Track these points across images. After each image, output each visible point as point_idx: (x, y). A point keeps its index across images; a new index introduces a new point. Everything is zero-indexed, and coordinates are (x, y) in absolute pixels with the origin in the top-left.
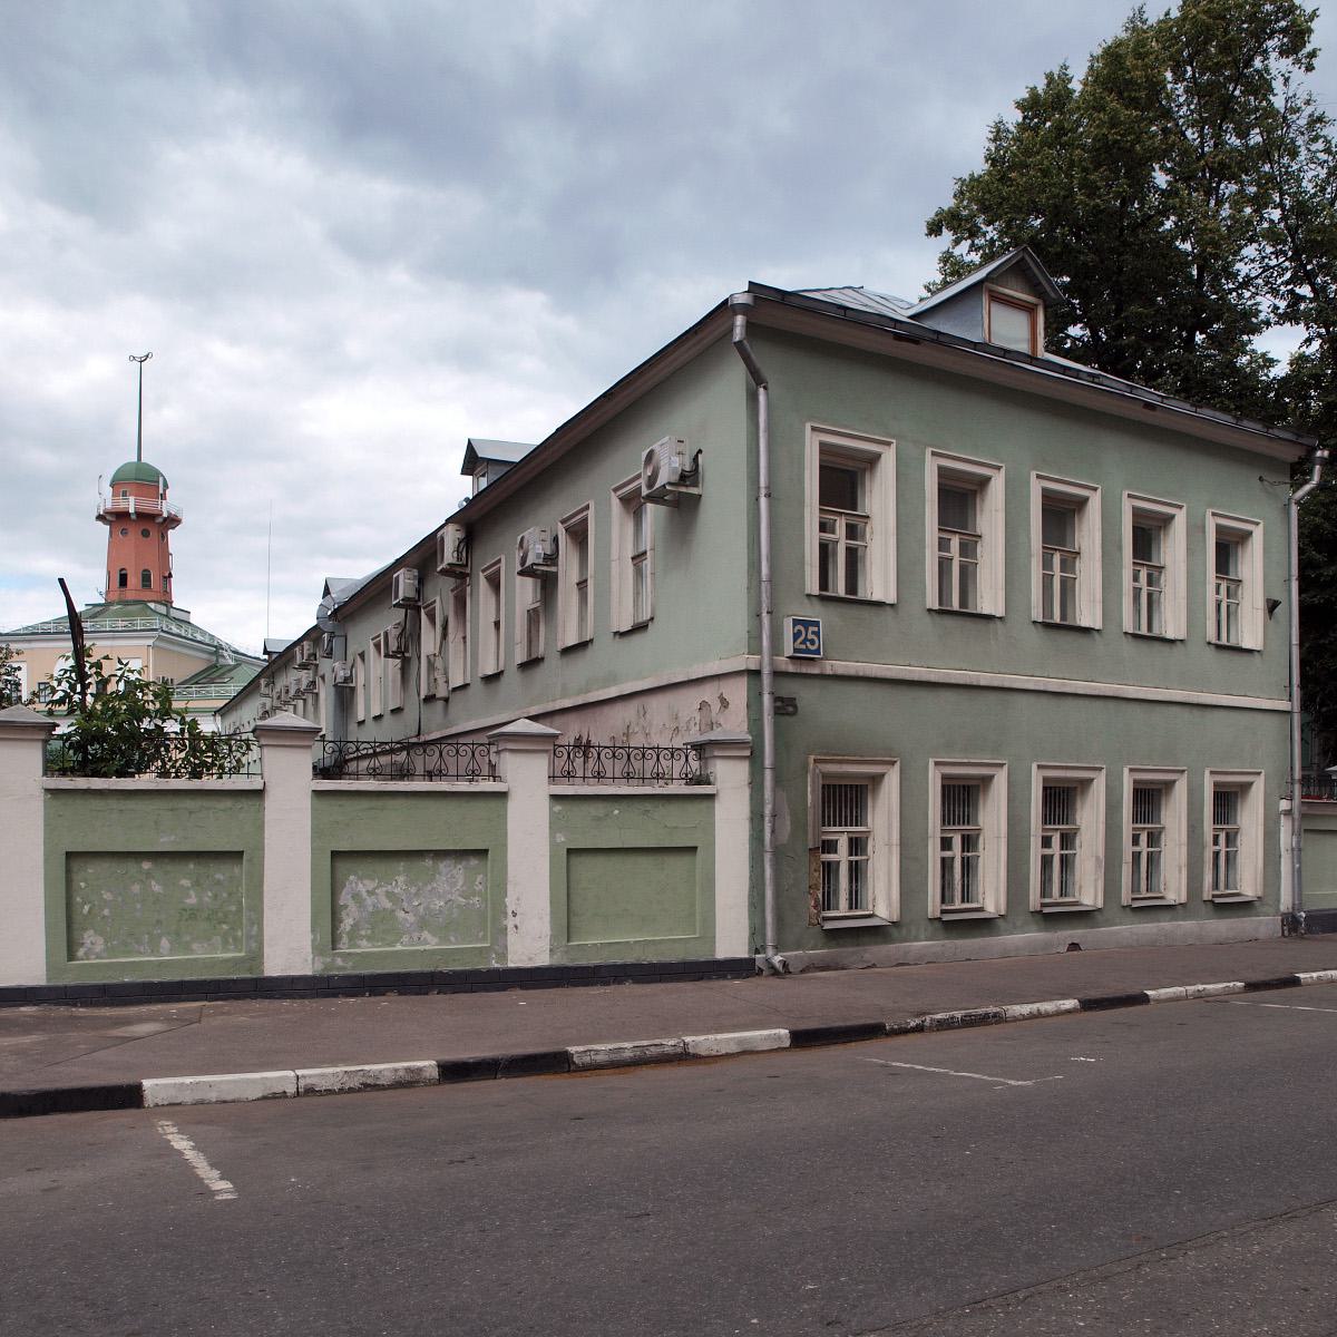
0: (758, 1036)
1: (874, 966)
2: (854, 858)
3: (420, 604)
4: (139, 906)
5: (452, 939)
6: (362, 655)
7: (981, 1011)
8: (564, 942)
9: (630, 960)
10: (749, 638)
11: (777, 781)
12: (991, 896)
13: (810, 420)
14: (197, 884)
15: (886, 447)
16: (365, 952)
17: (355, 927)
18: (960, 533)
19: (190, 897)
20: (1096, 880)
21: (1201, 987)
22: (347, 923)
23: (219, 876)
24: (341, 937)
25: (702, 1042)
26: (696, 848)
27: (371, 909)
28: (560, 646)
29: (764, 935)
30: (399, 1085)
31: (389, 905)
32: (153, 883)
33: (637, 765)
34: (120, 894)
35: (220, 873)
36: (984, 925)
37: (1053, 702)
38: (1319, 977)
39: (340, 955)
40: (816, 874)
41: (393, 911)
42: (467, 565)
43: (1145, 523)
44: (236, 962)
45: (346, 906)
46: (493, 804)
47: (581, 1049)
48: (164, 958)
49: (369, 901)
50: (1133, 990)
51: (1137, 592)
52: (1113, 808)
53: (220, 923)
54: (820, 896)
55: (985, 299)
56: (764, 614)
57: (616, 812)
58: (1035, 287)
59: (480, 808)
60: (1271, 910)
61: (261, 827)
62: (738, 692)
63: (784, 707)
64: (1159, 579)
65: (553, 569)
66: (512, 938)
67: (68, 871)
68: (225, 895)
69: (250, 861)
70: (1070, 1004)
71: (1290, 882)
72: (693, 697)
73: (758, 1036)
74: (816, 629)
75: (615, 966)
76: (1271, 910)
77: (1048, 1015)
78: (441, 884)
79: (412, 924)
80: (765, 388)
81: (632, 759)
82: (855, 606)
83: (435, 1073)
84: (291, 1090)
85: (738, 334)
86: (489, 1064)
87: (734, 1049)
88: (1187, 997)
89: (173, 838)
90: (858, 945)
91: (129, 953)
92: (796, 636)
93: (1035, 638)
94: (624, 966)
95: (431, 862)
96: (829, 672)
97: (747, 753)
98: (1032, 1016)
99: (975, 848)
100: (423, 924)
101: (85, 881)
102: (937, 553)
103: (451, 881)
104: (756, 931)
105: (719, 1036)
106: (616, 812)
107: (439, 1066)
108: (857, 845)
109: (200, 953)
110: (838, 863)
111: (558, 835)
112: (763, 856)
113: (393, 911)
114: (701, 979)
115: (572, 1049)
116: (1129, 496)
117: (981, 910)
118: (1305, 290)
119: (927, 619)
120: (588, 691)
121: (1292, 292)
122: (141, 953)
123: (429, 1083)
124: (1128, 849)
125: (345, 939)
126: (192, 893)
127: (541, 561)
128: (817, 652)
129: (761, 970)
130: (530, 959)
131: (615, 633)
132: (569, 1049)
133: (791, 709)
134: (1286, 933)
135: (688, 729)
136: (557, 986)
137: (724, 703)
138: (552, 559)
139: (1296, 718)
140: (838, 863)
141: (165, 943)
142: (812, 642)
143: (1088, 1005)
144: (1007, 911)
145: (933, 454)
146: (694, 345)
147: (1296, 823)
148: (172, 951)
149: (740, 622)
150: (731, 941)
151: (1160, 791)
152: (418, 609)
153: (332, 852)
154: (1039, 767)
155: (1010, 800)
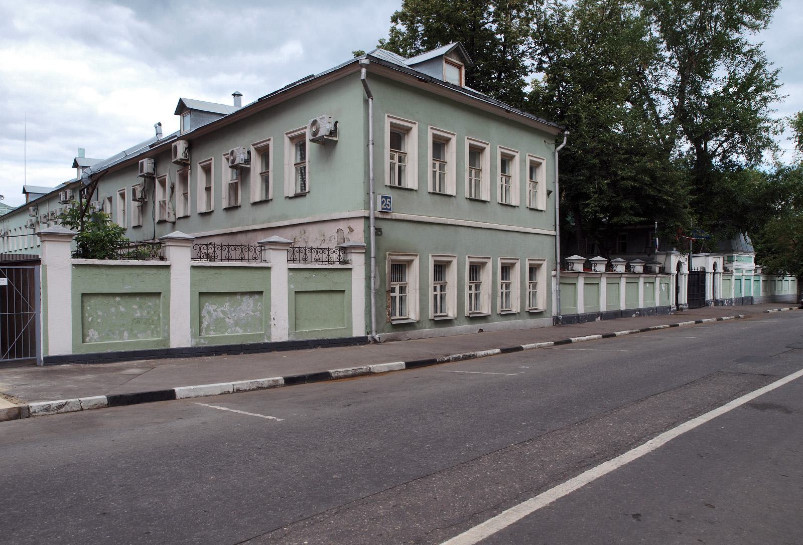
0: (732, 317)
1: (410, 339)
2: (401, 295)
3: (155, 176)
4: (114, 317)
5: (249, 330)
6: (110, 199)
7: (468, 354)
8: (294, 331)
9: (306, 339)
10: (364, 203)
11: (376, 263)
12: (451, 311)
13: (388, 113)
14: (140, 307)
15: (414, 125)
16: (213, 337)
17: (208, 325)
18: (439, 161)
19: (137, 313)
20: (489, 303)
21: (540, 344)
22: (205, 324)
23: (150, 304)
24: (203, 330)
25: (376, 367)
26: (344, 291)
27: (215, 318)
28: (252, 201)
29: (371, 327)
30: (270, 387)
31: (222, 316)
32: (121, 307)
33: (320, 255)
34: (106, 312)
35: (150, 302)
36: (448, 322)
37: (473, 230)
38: (578, 340)
39: (203, 338)
40: (389, 301)
41: (224, 318)
42: (188, 160)
43: (397, 131)
44: (157, 342)
45: (204, 317)
46: (265, 272)
47: (334, 371)
48: (124, 341)
49: (214, 314)
50: (517, 345)
51: (434, 172)
52: (494, 274)
53: (150, 325)
54: (390, 310)
55: (443, 62)
56: (371, 194)
57: (314, 275)
58: (462, 58)
59: (343, 274)
60: (549, 315)
61: (169, 282)
62: (359, 226)
63: (378, 232)
64: (405, 158)
65: (248, 166)
66: (273, 329)
67: (82, 302)
68: (153, 312)
69: (164, 297)
70: (497, 351)
71: (556, 304)
72: (334, 227)
73: (732, 317)
74: (389, 200)
75: (313, 341)
76: (549, 315)
77: (490, 355)
78: (244, 307)
79: (232, 324)
80: (372, 99)
81: (330, 253)
82: (406, 191)
83: (283, 382)
84: (231, 390)
85: (363, 76)
86: (302, 377)
87: (386, 370)
88: (535, 348)
89: (130, 287)
90: (404, 331)
91: (110, 339)
92: (383, 202)
93: (466, 205)
94: (318, 341)
95: (239, 297)
96: (394, 218)
97: (364, 251)
98: (588, 340)
99: (405, 292)
100: (236, 324)
101: (90, 306)
102: (432, 169)
103: (248, 304)
104: (368, 325)
105: (381, 365)
106: (314, 275)
107: (284, 379)
108: (402, 289)
109: (142, 338)
110: (395, 297)
111: (291, 285)
112: (370, 294)
113: (224, 318)
114: (347, 345)
115: (331, 371)
116: (500, 147)
117: (447, 316)
118: (545, 58)
119: (428, 196)
120: (269, 222)
121: (540, 59)
122: (115, 339)
123: (281, 386)
124: (499, 291)
125: (204, 331)
126: (138, 311)
127: (243, 162)
128: (390, 209)
129: (370, 341)
130: (280, 338)
131: (286, 197)
132: (329, 371)
133: (380, 233)
134: (555, 324)
135: (330, 240)
136: (291, 350)
137: (351, 230)
138: (248, 161)
139: (558, 238)
140: (395, 297)
141: (126, 334)
142: (389, 206)
143: (504, 351)
144: (521, 310)
145: (431, 128)
146: (335, 76)
147: (558, 280)
148: (129, 338)
149: (360, 196)
150: (358, 331)
151: (480, 266)
152: (154, 179)
153: (199, 293)
154: (469, 257)
155: (458, 271)
